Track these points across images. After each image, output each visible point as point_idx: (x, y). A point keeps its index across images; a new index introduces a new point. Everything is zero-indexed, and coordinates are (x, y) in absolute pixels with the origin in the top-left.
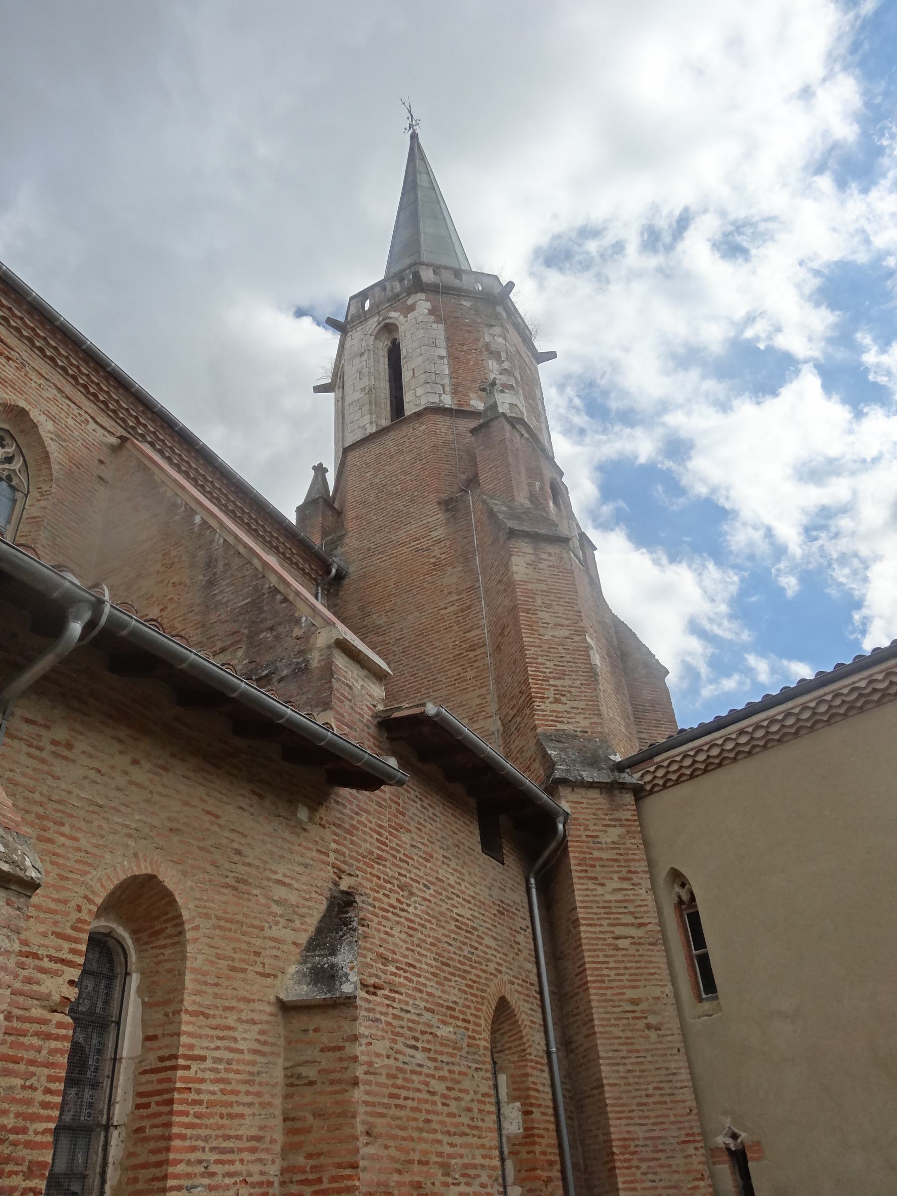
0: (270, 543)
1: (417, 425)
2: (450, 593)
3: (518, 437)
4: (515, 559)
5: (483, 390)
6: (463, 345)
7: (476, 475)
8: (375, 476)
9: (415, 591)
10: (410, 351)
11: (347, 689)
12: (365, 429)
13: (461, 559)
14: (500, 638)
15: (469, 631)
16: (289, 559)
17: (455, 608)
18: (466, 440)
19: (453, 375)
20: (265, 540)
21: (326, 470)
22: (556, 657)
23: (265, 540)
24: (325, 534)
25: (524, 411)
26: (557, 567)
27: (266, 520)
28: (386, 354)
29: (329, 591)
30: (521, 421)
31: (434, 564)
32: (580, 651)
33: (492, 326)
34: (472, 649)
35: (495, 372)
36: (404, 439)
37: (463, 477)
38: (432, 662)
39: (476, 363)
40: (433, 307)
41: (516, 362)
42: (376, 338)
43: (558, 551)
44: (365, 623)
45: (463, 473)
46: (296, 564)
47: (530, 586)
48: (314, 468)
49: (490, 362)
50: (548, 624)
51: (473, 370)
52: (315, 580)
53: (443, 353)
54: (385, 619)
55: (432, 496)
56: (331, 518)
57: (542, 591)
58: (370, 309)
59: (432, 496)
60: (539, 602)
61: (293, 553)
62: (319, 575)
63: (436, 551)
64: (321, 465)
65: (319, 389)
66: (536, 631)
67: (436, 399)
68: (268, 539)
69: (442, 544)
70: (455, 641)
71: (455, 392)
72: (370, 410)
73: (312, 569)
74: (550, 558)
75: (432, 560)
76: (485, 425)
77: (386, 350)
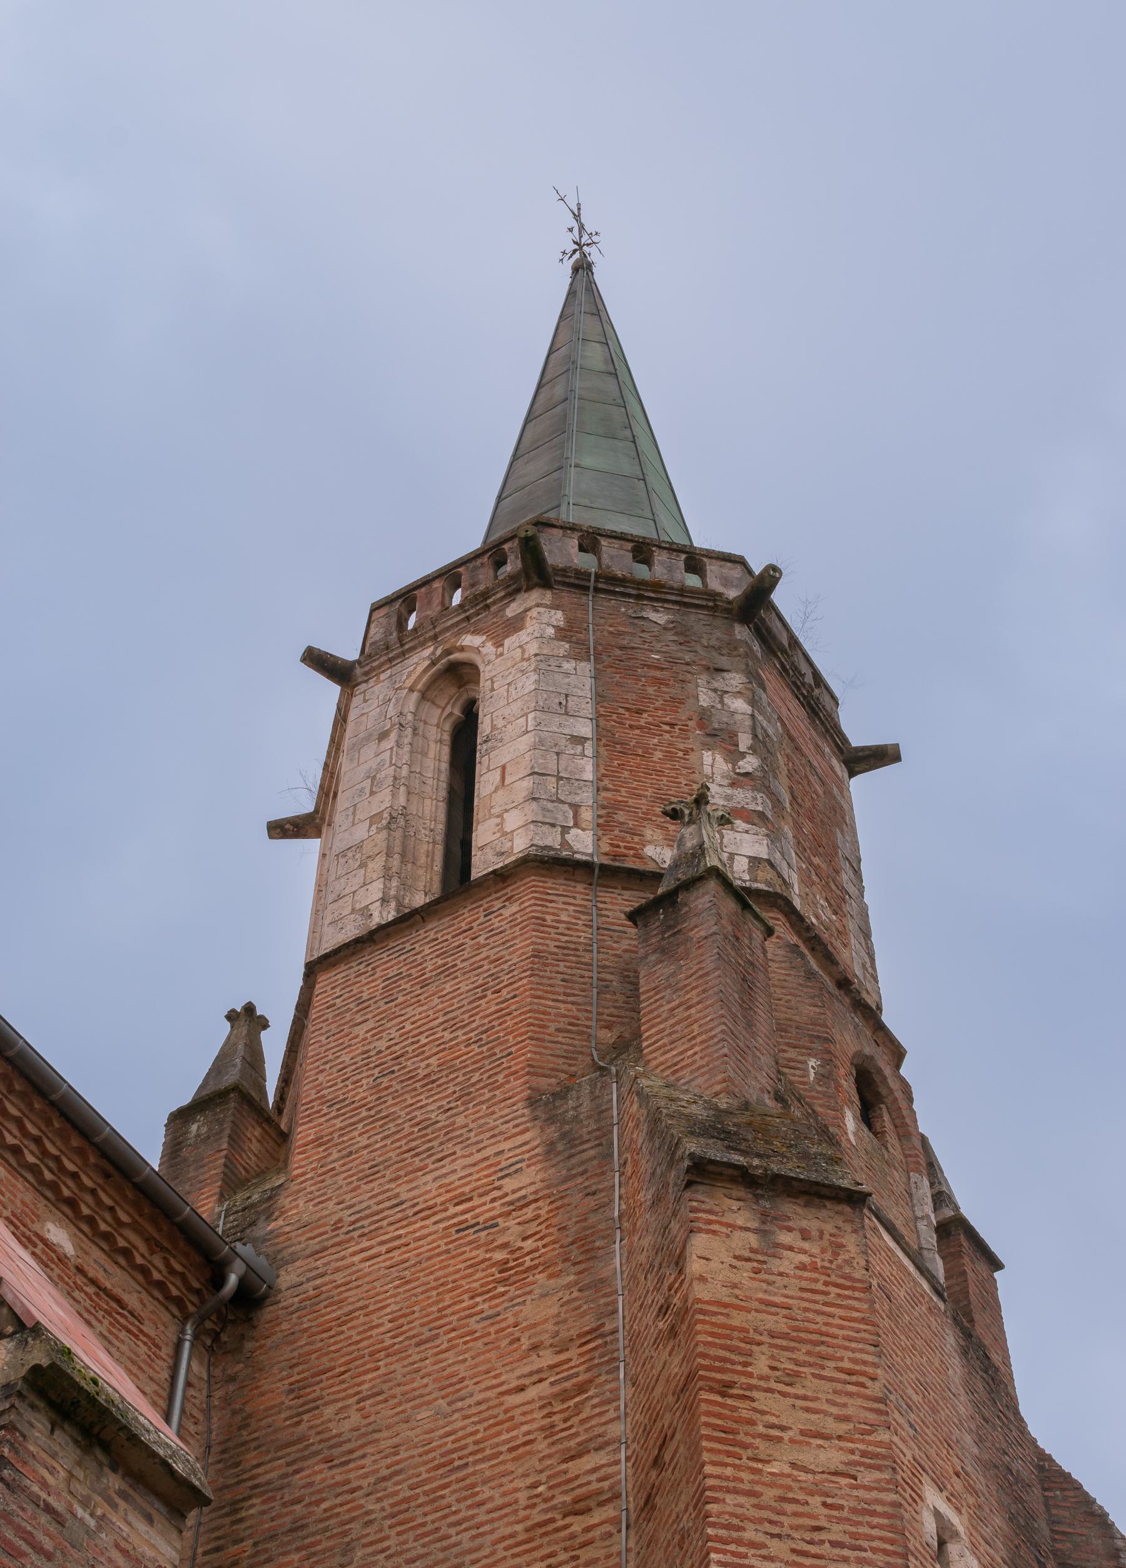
0: (54, 1187)
1: (498, 904)
2: (535, 1347)
3: (758, 935)
4: (699, 1243)
5: (675, 815)
6: (639, 712)
7: (637, 1035)
8: (377, 1034)
9: (443, 1342)
10: (500, 723)
11: (44, 1519)
12: (366, 912)
13: (575, 1253)
14: (654, 1474)
15: (579, 1455)
16: (107, 1237)
17: (544, 1389)
18: (625, 944)
19: (606, 782)
20: (42, 1181)
21: (264, 1024)
22: (797, 1528)
23: (42, 1181)
24: (232, 1183)
25: (794, 878)
26: (825, 1271)
27: (49, 1122)
28: (447, 737)
29: (216, 1338)
30: (779, 901)
31: (503, 1267)
32: (873, 1513)
33: (719, 670)
34: (578, 1508)
35: (718, 779)
36: (461, 939)
37: (608, 1037)
38: (467, 1545)
39: (670, 756)
40: (568, 621)
41: (781, 760)
42: (424, 696)
43: (829, 1228)
44: (303, 1427)
45: (609, 1027)
46: (127, 1253)
47: (737, 1319)
48: (232, 1016)
49: (707, 757)
50: (783, 1428)
51: (659, 773)
52: (179, 1302)
53: (585, 729)
54: (355, 1418)
55: (515, 1083)
56: (255, 1146)
57: (772, 1334)
58: (415, 629)
59: (515, 1083)
60: (761, 1365)
61: (120, 1223)
62: (190, 1289)
63: (511, 1230)
64: (249, 1009)
65: (282, 829)
66: (746, 1446)
67: (552, 839)
68: (48, 1176)
69: (529, 1212)
70: (535, 1486)
71: (604, 825)
72: (387, 868)
73: (172, 1271)
74: (806, 1245)
75: (499, 1256)
76: (670, 900)
77: (448, 727)
